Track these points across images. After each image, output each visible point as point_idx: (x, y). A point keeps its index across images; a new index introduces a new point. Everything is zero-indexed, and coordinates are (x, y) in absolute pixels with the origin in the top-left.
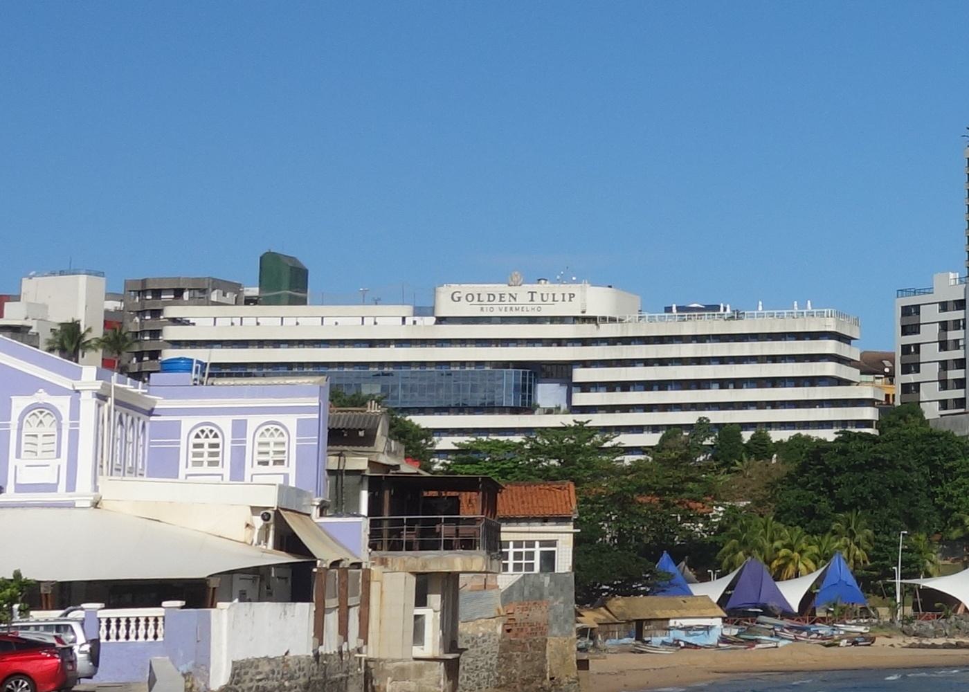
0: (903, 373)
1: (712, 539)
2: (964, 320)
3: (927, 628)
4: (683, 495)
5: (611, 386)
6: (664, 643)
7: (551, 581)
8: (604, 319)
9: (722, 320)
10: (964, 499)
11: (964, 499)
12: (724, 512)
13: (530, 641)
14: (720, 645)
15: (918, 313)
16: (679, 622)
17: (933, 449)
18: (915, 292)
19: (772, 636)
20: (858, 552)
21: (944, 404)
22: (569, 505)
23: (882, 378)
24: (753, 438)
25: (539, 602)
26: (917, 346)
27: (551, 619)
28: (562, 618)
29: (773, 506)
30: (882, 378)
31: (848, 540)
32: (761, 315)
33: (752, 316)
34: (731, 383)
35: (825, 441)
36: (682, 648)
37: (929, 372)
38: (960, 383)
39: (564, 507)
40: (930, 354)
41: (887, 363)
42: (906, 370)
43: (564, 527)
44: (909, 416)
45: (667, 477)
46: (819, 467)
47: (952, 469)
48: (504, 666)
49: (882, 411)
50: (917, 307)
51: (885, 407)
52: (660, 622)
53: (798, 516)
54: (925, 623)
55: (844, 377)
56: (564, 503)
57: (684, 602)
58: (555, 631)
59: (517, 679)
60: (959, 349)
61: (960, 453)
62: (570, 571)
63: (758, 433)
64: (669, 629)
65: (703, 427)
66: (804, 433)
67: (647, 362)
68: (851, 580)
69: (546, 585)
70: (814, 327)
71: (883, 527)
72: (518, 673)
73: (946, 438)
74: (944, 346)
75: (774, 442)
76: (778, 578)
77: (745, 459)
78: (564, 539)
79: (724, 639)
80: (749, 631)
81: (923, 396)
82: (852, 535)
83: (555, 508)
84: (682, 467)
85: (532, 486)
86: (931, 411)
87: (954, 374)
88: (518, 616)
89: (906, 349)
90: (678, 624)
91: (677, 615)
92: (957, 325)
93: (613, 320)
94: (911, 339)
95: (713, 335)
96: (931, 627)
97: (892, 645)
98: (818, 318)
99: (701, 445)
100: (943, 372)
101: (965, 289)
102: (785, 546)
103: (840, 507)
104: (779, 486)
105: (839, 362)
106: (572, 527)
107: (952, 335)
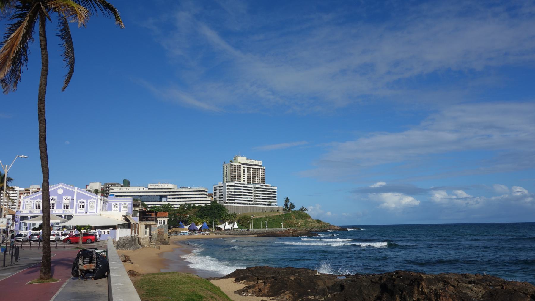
8: (172, 189)
18: (216, 185)
21: (220, 201)
26: (216, 193)
37: (218, 196)
38: (222, 198)
40: (218, 194)
42: (214, 196)
47: (221, 210)
51: (212, 201)
58: (165, 233)
65: (186, 204)
66: (200, 205)
67: (178, 195)
68: (207, 226)
70: (201, 190)
71: (211, 218)
74: (220, 192)
79: (189, 234)
80: (192, 233)
81: (217, 199)
82: (207, 219)
86: (218, 202)
87: (221, 196)
89: (214, 193)
92: (222, 190)
93: (173, 189)
94: (215, 192)
103: (205, 215)
107: (221, 191)
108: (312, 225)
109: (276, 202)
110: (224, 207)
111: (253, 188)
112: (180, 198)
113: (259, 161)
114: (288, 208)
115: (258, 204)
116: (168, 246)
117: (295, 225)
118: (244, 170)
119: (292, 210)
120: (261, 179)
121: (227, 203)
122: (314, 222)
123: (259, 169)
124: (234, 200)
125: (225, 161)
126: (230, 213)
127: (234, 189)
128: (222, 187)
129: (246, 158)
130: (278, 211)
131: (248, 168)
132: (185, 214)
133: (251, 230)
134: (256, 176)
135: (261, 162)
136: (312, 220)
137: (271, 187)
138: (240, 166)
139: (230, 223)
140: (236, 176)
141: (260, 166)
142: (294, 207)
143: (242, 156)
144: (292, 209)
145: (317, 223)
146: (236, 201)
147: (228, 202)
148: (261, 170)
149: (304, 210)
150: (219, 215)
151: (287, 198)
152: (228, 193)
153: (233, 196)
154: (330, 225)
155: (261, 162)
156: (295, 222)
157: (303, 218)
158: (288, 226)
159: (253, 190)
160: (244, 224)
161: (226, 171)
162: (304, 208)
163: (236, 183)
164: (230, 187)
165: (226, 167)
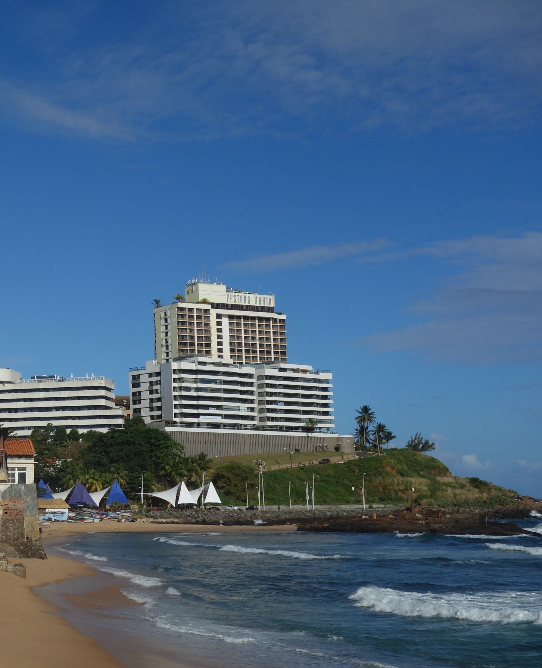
0: (133, 404)
1: (57, 475)
2: (160, 381)
3: (157, 514)
4: (44, 456)
5: (10, 410)
6: (44, 519)
7: (25, 488)
8: (6, 382)
9: (56, 382)
10: (165, 458)
11: (165, 458)
12: (62, 463)
13: (16, 518)
14: (69, 520)
15: (139, 378)
16: (50, 510)
17: (150, 437)
18: (138, 369)
19: (90, 517)
20: (122, 481)
21: (152, 417)
22: (31, 449)
23: (122, 407)
24: (71, 432)
25: (19, 499)
26: (139, 393)
27: (26, 507)
28: (31, 507)
29: (82, 461)
30: (122, 407)
31: (117, 475)
32: (72, 380)
33: (69, 380)
34: (60, 409)
35: (102, 433)
36: (53, 521)
37: (145, 404)
38: (159, 408)
39: (29, 451)
40: (146, 395)
41: (124, 401)
42: (135, 403)
43: (30, 461)
44: (138, 422)
45: (37, 448)
46: (102, 444)
47: (159, 445)
48: (4, 531)
49: (126, 421)
50: (139, 376)
51: (126, 418)
52: (42, 510)
53: (94, 465)
54: (156, 512)
55: (109, 406)
56: (28, 449)
57: (52, 501)
58: (28, 514)
59: (11, 538)
60: (158, 393)
61: (162, 438)
62: (33, 483)
63: (73, 430)
64: (46, 513)
65: (49, 428)
66: (93, 429)
67: (25, 400)
68: (122, 493)
69: (22, 490)
70: (95, 384)
71: (131, 470)
72: (11, 535)
73: (156, 432)
74: (151, 392)
75: (80, 433)
76: (89, 490)
77: (68, 441)
78: (30, 467)
79: (70, 518)
80: (79, 514)
81: (143, 414)
82: (119, 474)
83: (25, 451)
84: (43, 444)
85: (11, 441)
86: (147, 421)
87: (156, 404)
88: (10, 505)
89: (134, 394)
90: (50, 511)
91: (49, 507)
92: (157, 383)
93: (10, 382)
94: (136, 390)
95: (52, 388)
96: (158, 514)
97: (143, 522)
98: (97, 381)
99: (49, 435)
100: (151, 404)
101: (160, 367)
102: (91, 478)
103: (112, 462)
104: (85, 452)
105: (106, 399)
106: (34, 460)
107: (155, 387)
108: (455, 495)
109: (330, 422)
110: (167, 436)
111: (255, 376)
112: (31, 410)
113: (266, 296)
114: (368, 441)
115: (272, 428)
116: (41, 560)
117: (400, 494)
118: (219, 324)
119: (384, 447)
120: (273, 350)
121: (174, 424)
122: (463, 486)
123: (268, 319)
124: (197, 416)
125: (158, 299)
126: (187, 455)
127: (196, 381)
128: (158, 374)
129: (223, 288)
130: (337, 449)
131: (231, 317)
132: (49, 458)
133: (260, 507)
134: (258, 343)
135: (272, 297)
136: (455, 478)
137: (311, 373)
138: (206, 311)
139: (192, 486)
140: (196, 342)
141: (270, 310)
142: (389, 437)
143: (212, 282)
144: (382, 443)
145: (472, 488)
146: (202, 419)
147: (178, 420)
148: (271, 324)
149: (423, 447)
150: (155, 461)
151: (366, 409)
152: (176, 394)
153: (195, 403)
154: (519, 498)
155: (272, 297)
156: (398, 485)
157: (421, 473)
158: (377, 498)
159: (256, 385)
160: (232, 489)
161: (163, 329)
162: (423, 441)
163: (200, 363)
164: (183, 376)
165: (163, 315)
